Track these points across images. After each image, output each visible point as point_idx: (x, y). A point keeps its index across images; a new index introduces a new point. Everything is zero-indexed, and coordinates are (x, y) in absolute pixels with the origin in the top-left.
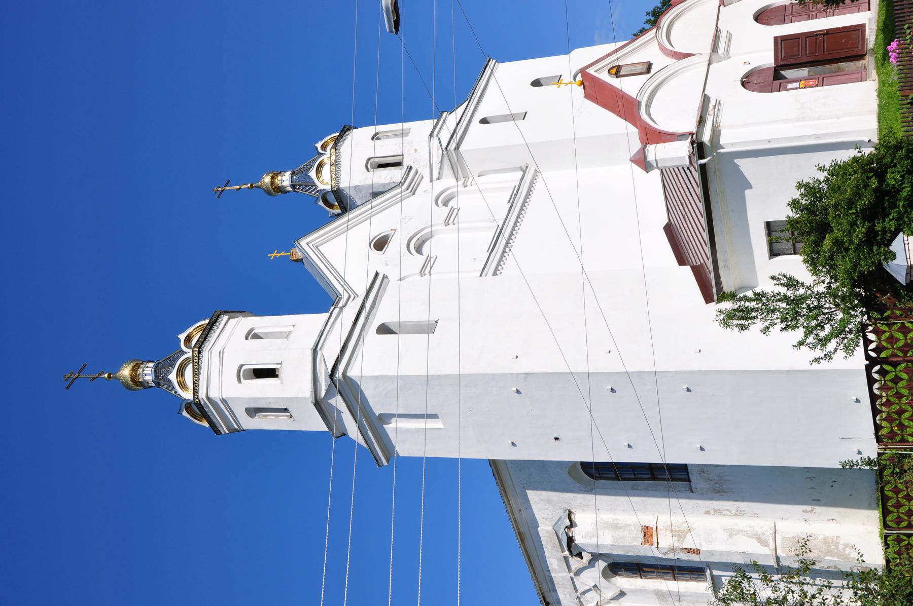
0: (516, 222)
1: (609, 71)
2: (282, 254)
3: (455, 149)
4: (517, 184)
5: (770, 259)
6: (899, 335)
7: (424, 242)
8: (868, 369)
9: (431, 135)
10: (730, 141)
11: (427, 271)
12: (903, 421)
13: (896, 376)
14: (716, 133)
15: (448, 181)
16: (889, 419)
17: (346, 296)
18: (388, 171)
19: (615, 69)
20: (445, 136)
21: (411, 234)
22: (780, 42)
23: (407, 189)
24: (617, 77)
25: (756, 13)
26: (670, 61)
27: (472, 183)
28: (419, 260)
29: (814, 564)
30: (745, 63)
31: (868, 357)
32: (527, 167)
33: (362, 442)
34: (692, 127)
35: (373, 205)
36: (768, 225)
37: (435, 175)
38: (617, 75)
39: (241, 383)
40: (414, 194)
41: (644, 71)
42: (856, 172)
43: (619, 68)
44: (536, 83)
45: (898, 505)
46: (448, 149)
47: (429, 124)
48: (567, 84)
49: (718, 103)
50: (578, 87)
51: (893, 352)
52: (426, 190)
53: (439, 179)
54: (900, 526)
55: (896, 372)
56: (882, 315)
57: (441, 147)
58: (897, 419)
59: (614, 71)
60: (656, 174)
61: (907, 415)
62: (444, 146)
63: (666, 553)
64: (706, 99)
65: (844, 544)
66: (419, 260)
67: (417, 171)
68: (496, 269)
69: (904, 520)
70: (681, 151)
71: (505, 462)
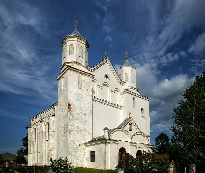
2: (76, 26)
4: (120, 105)
7: (107, 86)
9: (131, 87)
10: (109, 146)
11: (98, 87)
14: (109, 143)
15: (122, 91)
17: (93, 69)
18: (85, 48)
20: (131, 90)
21: (119, 89)
28: (114, 90)
29: (164, 133)
37: (123, 88)
38: (129, 124)
44: (142, 109)
47: (135, 87)
59: (130, 124)
62: (128, 90)
63: (114, 130)
66: (114, 90)
67: (124, 84)
71: (56, 103)
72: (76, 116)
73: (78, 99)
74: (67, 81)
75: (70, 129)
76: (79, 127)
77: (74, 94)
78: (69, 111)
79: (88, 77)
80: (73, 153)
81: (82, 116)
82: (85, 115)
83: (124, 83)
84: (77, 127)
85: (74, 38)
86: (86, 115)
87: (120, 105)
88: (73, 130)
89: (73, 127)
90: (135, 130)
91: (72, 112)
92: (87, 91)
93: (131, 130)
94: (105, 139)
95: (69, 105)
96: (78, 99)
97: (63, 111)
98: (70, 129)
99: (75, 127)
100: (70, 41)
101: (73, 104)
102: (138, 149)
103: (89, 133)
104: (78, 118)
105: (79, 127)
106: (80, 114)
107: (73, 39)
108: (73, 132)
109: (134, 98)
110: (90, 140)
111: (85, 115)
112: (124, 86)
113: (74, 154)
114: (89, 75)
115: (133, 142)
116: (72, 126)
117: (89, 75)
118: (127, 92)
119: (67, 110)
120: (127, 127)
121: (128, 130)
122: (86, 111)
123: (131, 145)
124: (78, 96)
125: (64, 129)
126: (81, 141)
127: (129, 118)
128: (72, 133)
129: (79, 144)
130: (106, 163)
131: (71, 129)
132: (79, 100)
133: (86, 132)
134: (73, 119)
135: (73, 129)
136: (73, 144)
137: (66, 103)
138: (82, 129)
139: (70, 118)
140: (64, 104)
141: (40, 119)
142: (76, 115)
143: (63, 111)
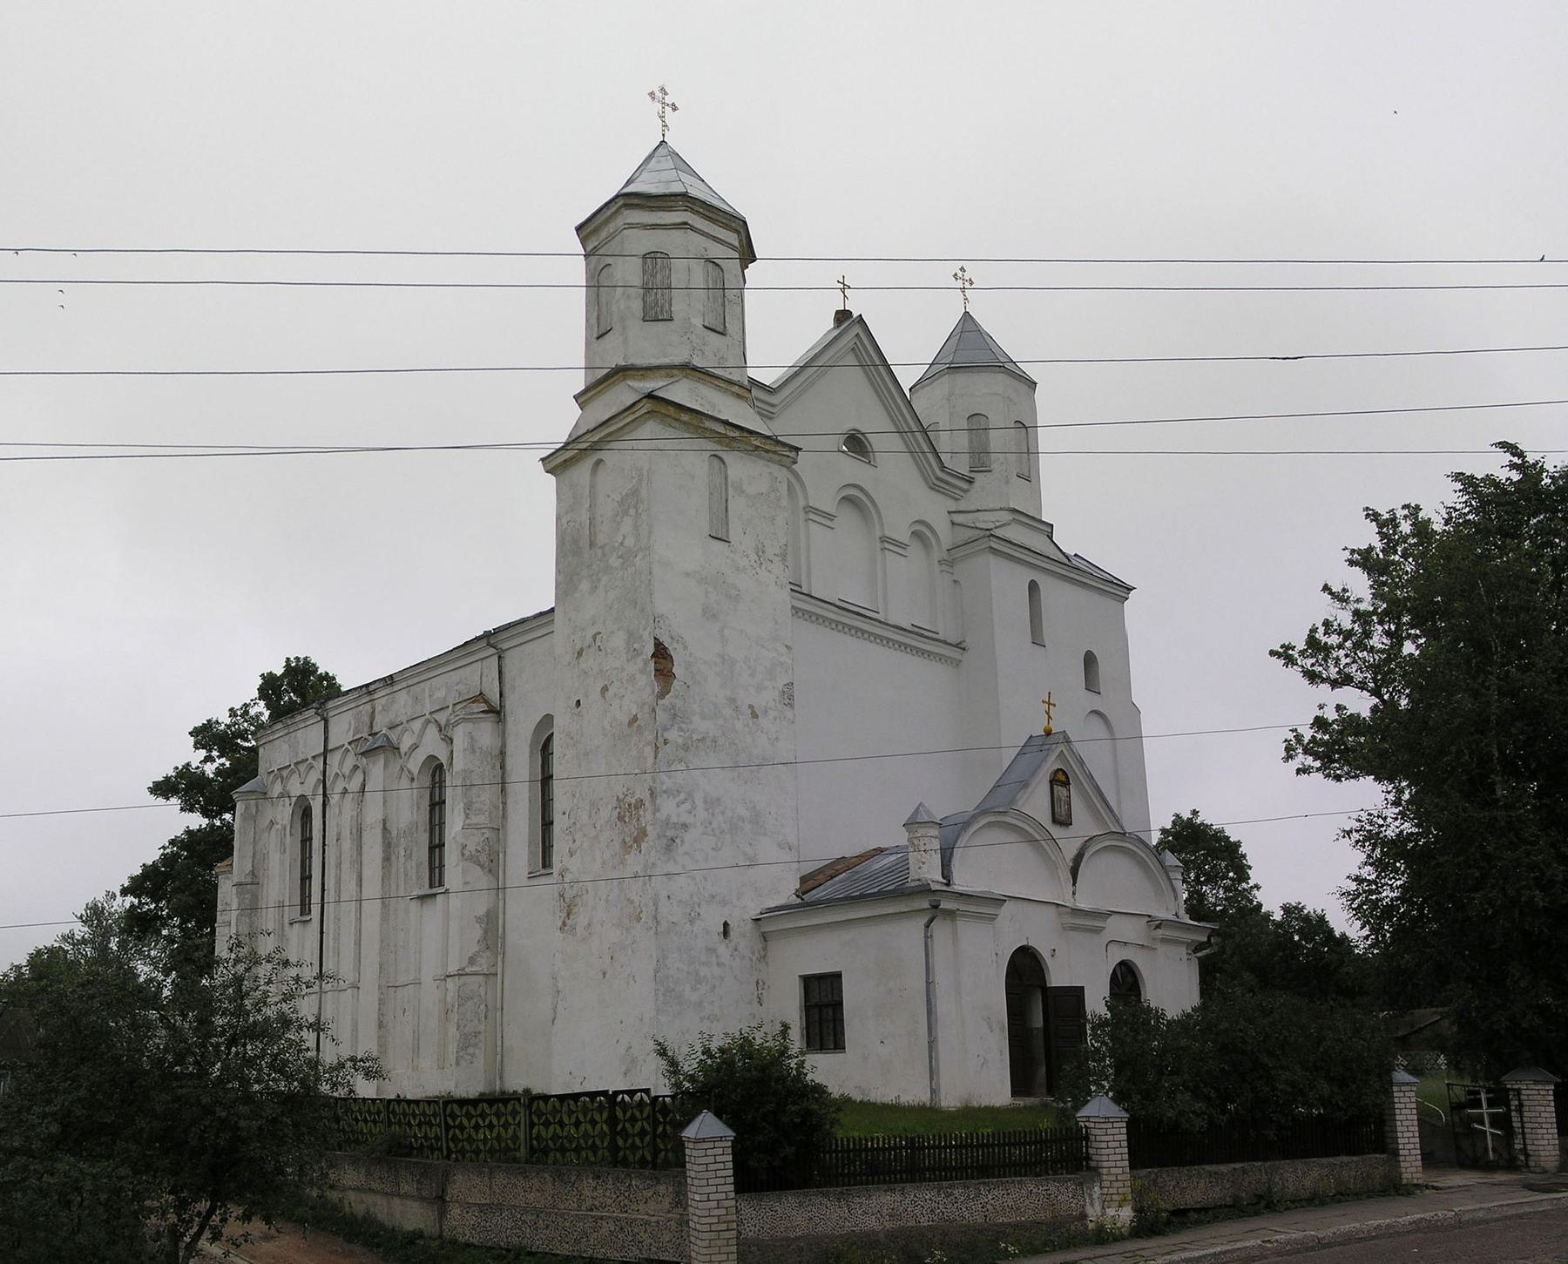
0: (882, 638)
1: (1059, 770)
3: (991, 547)
5: (800, 976)
6: (638, 1125)
8: (605, 1093)
12: (553, 1126)
13: (597, 1123)
14: (951, 914)
16: (555, 1111)
19: (1063, 778)
22: (1077, 994)
23: (938, 479)
24: (1051, 781)
25: (1135, 964)
26: (1070, 852)
27: (944, 573)
30: (1054, 950)
31: (616, 1093)
32: (964, 649)
33: (576, 451)
34: (960, 885)
35: (916, 433)
36: (837, 976)
37: (959, 518)
38: (1053, 782)
39: (163, 789)
40: (933, 488)
41: (1057, 816)
42: (1398, 1065)
43: (1066, 784)
45: (498, 1115)
46: (991, 538)
48: (1048, 713)
49: (992, 918)
50: (1043, 728)
51: (621, 1121)
52: (935, 509)
53: (953, 523)
54: (448, 1118)
55: (484, 1127)
56: (659, 1111)
57: (996, 527)
58: (554, 1120)
59: (1061, 777)
60: (902, 838)
61: (558, 1130)
62: (998, 532)
64: (999, 901)
65: (474, 1053)
68: (805, 612)
69: (454, 1122)
70: (930, 871)
72: (702, 726)
73: (710, 614)
74: (635, 492)
75: (669, 816)
76: (719, 800)
77: (688, 575)
78: (663, 694)
79: (763, 458)
80: (694, 989)
81: (739, 725)
82: (755, 715)
83: (965, 486)
84: (712, 803)
85: (669, 209)
86: (761, 720)
87: (941, 637)
88: (685, 826)
89: (687, 806)
90: (1084, 825)
91: (679, 703)
92: (760, 551)
93: (1062, 819)
94: (925, 890)
95: (661, 653)
96: (710, 614)
97: (605, 689)
98: (669, 816)
99: (699, 803)
100: (645, 227)
101: (685, 648)
102: (1118, 955)
103: (779, 846)
104: (714, 741)
105: (719, 800)
106: (728, 712)
107: (661, 214)
108: (689, 836)
109: (1033, 587)
110: (786, 892)
111: (755, 715)
112: (962, 506)
113: (694, 997)
114: (767, 451)
115: (1083, 905)
116: (682, 796)
117: (767, 451)
118: (993, 551)
119: (646, 681)
120: (1037, 803)
121: (1044, 817)
122: (760, 688)
123: (1075, 928)
124: (710, 589)
125: (621, 818)
126: (739, 899)
127: (1048, 733)
128: (681, 850)
129: (726, 925)
130: (937, 1060)
131: (674, 819)
132: (715, 616)
133: (765, 834)
134: (686, 748)
135: (688, 819)
136: (692, 922)
137: (632, 636)
138: (741, 819)
139: (666, 742)
140: (618, 641)
141: (357, 731)
142: (704, 718)
143: (605, 689)
